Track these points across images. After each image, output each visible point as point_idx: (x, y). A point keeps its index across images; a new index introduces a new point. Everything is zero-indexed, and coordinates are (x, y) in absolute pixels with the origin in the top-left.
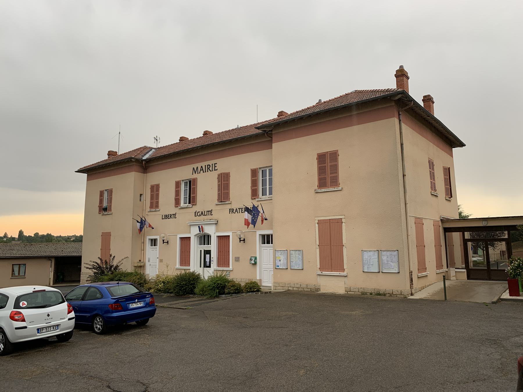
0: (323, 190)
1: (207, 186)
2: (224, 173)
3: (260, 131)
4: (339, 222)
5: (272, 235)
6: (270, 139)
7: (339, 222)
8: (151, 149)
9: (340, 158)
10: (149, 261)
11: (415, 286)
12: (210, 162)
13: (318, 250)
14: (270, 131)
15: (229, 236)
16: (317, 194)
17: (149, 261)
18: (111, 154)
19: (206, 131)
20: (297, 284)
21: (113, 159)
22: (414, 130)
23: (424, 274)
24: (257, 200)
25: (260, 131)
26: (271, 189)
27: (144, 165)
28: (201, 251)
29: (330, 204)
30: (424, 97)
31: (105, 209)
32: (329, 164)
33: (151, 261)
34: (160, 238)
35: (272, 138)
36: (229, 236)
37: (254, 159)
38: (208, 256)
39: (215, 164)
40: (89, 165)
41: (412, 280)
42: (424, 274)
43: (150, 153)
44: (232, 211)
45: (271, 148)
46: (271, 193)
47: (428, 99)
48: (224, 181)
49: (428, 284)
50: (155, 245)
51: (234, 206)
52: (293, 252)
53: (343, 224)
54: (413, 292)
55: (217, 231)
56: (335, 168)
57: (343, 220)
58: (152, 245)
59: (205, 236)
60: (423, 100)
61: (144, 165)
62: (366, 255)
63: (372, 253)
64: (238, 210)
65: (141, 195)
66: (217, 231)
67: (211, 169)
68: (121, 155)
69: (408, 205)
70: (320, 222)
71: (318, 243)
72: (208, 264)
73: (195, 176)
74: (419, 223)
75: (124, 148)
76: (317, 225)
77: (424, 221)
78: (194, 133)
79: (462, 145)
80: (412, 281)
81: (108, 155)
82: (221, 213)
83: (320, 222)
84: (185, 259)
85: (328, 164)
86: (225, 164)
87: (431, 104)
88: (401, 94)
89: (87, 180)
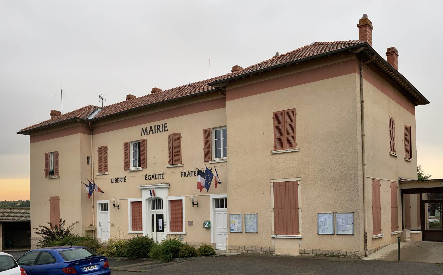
0: (280, 151)
1: (157, 149)
2: (175, 134)
4: (295, 184)
5: (226, 199)
7: (295, 184)
8: (97, 108)
9: (297, 118)
10: (100, 226)
12: (160, 123)
13: (273, 214)
14: (223, 88)
15: (181, 200)
16: (273, 156)
17: (100, 226)
18: (54, 113)
19: (155, 88)
20: (252, 247)
24: (210, 162)
26: (225, 151)
28: (153, 215)
29: (286, 166)
30: (389, 49)
31: (52, 173)
32: (286, 124)
33: (102, 226)
34: (111, 202)
35: (225, 95)
36: (181, 200)
37: (206, 119)
38: (160, 220)
39: (165, 124)
41: (366, 242)
43: (96, 113)
44: (184, 174)
45: (225, 106)
46: (225, 155)
47: (392, 52)
48: (175, 142)
50: (105, 210)
51: (187, 169)
52: (248, 216)
53: (299, 186)
54: (367, 253)
55: (169, 195)
56: (292, 128)
57: (299, 183)
58: (102, 210)
60: (386, 53)
62: (321, 218)
63: (327, 215)
64: (191, 173)
66: (169, 195)
67: (161, 129)
68: (65, 115)
69: (365, 167)
70: (276, 185)
72: (160, 228)
73: (144, 137)
74: (376, 184)
75: (67, 108)
76: (272, 188)
77: (381, 183)
78: (142, 91)
79: (425, 102)
82: (173, 176)
83: (276, 185)
85: (285, 123)
86: (176, 124)
89: (30, 143)
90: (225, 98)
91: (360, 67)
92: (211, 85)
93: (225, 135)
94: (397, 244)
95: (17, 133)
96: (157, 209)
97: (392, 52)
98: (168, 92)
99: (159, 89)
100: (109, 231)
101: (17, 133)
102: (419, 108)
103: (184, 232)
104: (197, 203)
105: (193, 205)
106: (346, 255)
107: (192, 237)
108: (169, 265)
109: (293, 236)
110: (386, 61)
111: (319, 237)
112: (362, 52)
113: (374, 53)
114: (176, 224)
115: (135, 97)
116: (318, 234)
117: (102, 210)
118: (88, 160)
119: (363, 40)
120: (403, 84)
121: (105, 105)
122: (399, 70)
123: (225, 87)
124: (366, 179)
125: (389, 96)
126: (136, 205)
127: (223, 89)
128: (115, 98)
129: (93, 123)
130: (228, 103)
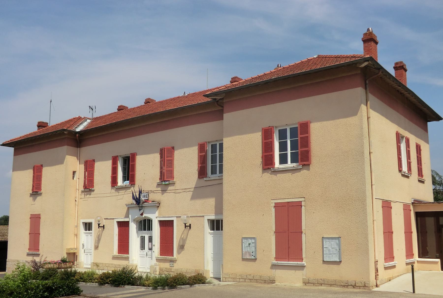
3: (209, 99)
4: (299, 205)
5: (222, 221)
6: (221, 108)
7: (299, 205)
8: (85, 119)
11: (380, 277)
14: (220, 99)
18: (41, 125)
19: (149, 99)
20: (250, 275)
21: (44, 131)
22: (382, 101)
23: (391, 264)
24: (205, 179)
25: (209, 99)
26: (221, 167)
27: (77, 138)
29: (289, 184)
30: (396, 64)
33: (85, 248)
34: (95, 221)
35: (223, 107)
37: (203, 131)
40: (16, 137)
41: (377, 270)
42: (391, 264)
43: (85, 124)
45: (222, 119)
46: (221, 171)
47: (400, 67)
49: (397, 275)
50: (89, 230)
53: (303, 207)
54: (378, 283)
56: (306, 142)
57: (303, 204)
58: (86, 230)
59: (145, 220)
60: (394, 68)
61: (77, 138)
65: (74, 173)
68: (52, 126)
69: (374, 187)
70: (277, 206)
71: (303, 236)
74: (387, 206)
75: (55, 120)
77: (393, 205)
78: (134, 101)
79: (438, 118)
80: (377, 271)
81: (39, 126)
83: (13, 170)
84: (124, 247)
87: (404, 72)
88: (368, 61)
90: (223, 110)
91: (365, 82)
92: (208, 97)
93: (221, 150)
94: (411, 274)
95: (1, 145)
96: (145, 230)
97: (400, 67)
98: (161, 102)
99: (153, 100)
100: (93, 254)
101: (1, 145)
102: (431, 125)
104: (190, 225)
105: (186, 226)
106: (355, 286)
107: (183, 264)
110: (394, 76)
111: (326, 266)
112: (366, 67)
113: (380, 68)
114: (167, 247)
115: (127, 108)
116: (323, 261)
117: (86, 230)
118: (73, 175)
119: (368, 54)
120: (412, 99)
121: (95, 116)
122: (408, 86)
123: (222, 99)
124: (374, 199)
125: (398, 111)
126: (123, 226)
127: (220, 101)
128: (106, 108)
129: (81, 135)
130: (225, 115)
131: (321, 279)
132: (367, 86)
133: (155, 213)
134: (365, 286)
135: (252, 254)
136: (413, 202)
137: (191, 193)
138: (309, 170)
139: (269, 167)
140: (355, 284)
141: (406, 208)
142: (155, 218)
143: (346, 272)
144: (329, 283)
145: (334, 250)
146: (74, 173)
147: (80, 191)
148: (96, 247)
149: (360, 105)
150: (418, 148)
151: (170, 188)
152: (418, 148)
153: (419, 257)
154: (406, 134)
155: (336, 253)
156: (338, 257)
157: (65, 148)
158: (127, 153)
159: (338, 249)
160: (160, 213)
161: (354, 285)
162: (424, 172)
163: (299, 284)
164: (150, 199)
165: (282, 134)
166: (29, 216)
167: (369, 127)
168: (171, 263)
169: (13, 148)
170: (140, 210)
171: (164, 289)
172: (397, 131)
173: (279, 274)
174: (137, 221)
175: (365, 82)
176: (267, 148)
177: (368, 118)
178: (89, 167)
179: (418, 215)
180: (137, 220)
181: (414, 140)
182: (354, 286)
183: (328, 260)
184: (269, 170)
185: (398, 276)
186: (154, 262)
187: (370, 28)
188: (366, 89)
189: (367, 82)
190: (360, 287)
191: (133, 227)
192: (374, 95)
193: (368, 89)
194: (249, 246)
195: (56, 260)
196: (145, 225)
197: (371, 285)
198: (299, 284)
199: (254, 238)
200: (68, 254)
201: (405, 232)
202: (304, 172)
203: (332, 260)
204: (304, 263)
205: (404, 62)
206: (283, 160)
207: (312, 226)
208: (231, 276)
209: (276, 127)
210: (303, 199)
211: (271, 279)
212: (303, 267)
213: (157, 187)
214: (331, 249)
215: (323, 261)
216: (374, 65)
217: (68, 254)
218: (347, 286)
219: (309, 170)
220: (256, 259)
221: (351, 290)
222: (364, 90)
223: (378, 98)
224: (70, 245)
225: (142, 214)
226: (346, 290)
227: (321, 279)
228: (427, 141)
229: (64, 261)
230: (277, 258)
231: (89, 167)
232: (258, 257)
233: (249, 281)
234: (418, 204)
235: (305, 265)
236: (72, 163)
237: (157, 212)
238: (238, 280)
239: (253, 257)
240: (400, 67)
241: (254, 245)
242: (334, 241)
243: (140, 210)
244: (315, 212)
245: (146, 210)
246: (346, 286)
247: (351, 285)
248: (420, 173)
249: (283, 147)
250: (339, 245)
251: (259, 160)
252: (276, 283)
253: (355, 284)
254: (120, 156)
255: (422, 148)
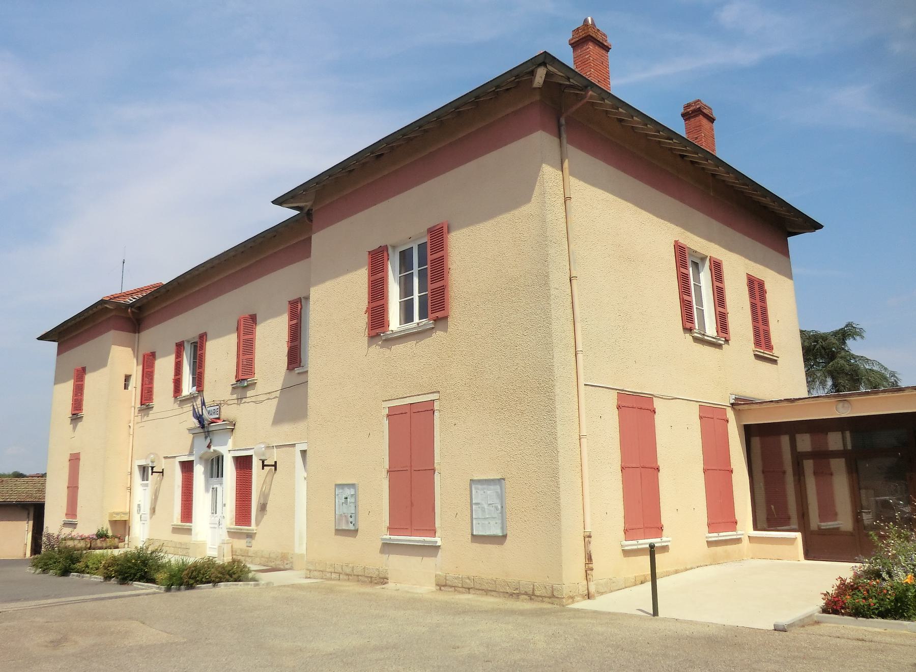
4: (427, 409)
7: (427, 409)
29: (414, 367)
30: (688, 106)
33: (142, 512)
54: (592, 589)
57: (437, 406)
58: (143, 480)
60: (683, 115)
69: (580, 356)
70: (393, 414)
77: (658, 404)
79: (814, 226)
87: (705, 121)
103: (253, 526)
106: (533, 594)
108: (67, 603)
109: (634, 542)
111: (477, 547)
120: (730, 179)
122: (721, 153)
126: (187, 467)
131: (469, 578)
132: (563, 128)
133: (225, 444)
134: (553, 596)
135: (351, 520)
136: (732, 401)
137: (276, 401)
138: (445, 330)
139: (378, 331)
140: (533, 590)
141: (710, 417)
142: (228, 450)
143: (513, 563)
144: (483, 587)
145: (493, 509)
146: (127, 378)
147: (137, 410)
148: (153, 510)
149: (539, 169)
150: (756, 288)
151: (250, 393)
152: (756, 288)
153: (756, 528)
154: (696, 243)
155: (496, 515)
156: (500, 526)
157: (112, 334)
158: (191, 334)
159: (499, 507)
160: (234, 443)
161: (530, 593)
162: (776, 337)
163: (426, 589)
164: (222, 417)
165: (405, 259)
166: (68, 457)
167: (569, 219)
168: (249, 540)
169: (56, 344)
170: (206, 438)
171: (179, 590)
172: (676, 242)
173: (396, 563)
174: (206, 461)
175: (559, 121)
176: (377, 291)
177: (566, 199)
178: (148, 362)
179: (749, 432)
180: (206, 457)
181: (738, 268)
182: (532, 596)
183: (481, 533)
184: (377, 338)
185: (677, 572)
186: (226, 537)
187: (589, 19)
188: (560, 137)
189: (563, 121)
190: (542, 598)
191: (199, 471)
192: (581, 147)
193: (564, 136)
194: (346, 503)
195: (86, 534)
196: (215, 465)
197: (566, 592)
198: (426, 589)
199: (353, 486)
200: (114, 523)
201: (705, 471)
202: (438, 334)
203: (488, 533)
204: (438, 540)
205: (705, 102)
206: (407, 315)
207: (457, 455)
208: (318, 568)
209: (394, 247)
210: (434, 396)
211: (381, 576)
212: (434, 549)
213: (232, 394)
214: (486, 506)
215: (472, 535)
216: (568, 79)
217: (114, 523)
218: (518, 595)
219: (445, 330)
220: (356, 531)
221: (525, 605)
222: (556, 140)
223: (606, 160)
224: (117, 507)
225: (209, 447)
226: (512, 604)
227: (469, 578)
228: (787, 273)
229: (102, 536)
230: (392, 529)
231: (148, 362)
232: (361, 526)
233: (346, 577)
234: (746, 407)
235: (438, 544)
236: (121, 358)
237: (230, 441)
238: (328, 575)
239: (351, 527)
240: (694, 111)
241: (353, 500)
242: (492, 487)
243: (206, 438)
244: (456, 422)
245: (216, 438)
246: (515, 595)
247: (526, 594)
248: (762, 337)
249: (406, 290)
250: (501, 497)
251: (363, 321)
252: (391, 585)
253: (533, 590)
254: (188, 341)
255: (767, 286)
